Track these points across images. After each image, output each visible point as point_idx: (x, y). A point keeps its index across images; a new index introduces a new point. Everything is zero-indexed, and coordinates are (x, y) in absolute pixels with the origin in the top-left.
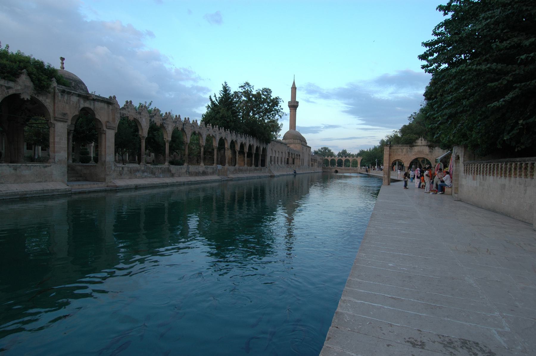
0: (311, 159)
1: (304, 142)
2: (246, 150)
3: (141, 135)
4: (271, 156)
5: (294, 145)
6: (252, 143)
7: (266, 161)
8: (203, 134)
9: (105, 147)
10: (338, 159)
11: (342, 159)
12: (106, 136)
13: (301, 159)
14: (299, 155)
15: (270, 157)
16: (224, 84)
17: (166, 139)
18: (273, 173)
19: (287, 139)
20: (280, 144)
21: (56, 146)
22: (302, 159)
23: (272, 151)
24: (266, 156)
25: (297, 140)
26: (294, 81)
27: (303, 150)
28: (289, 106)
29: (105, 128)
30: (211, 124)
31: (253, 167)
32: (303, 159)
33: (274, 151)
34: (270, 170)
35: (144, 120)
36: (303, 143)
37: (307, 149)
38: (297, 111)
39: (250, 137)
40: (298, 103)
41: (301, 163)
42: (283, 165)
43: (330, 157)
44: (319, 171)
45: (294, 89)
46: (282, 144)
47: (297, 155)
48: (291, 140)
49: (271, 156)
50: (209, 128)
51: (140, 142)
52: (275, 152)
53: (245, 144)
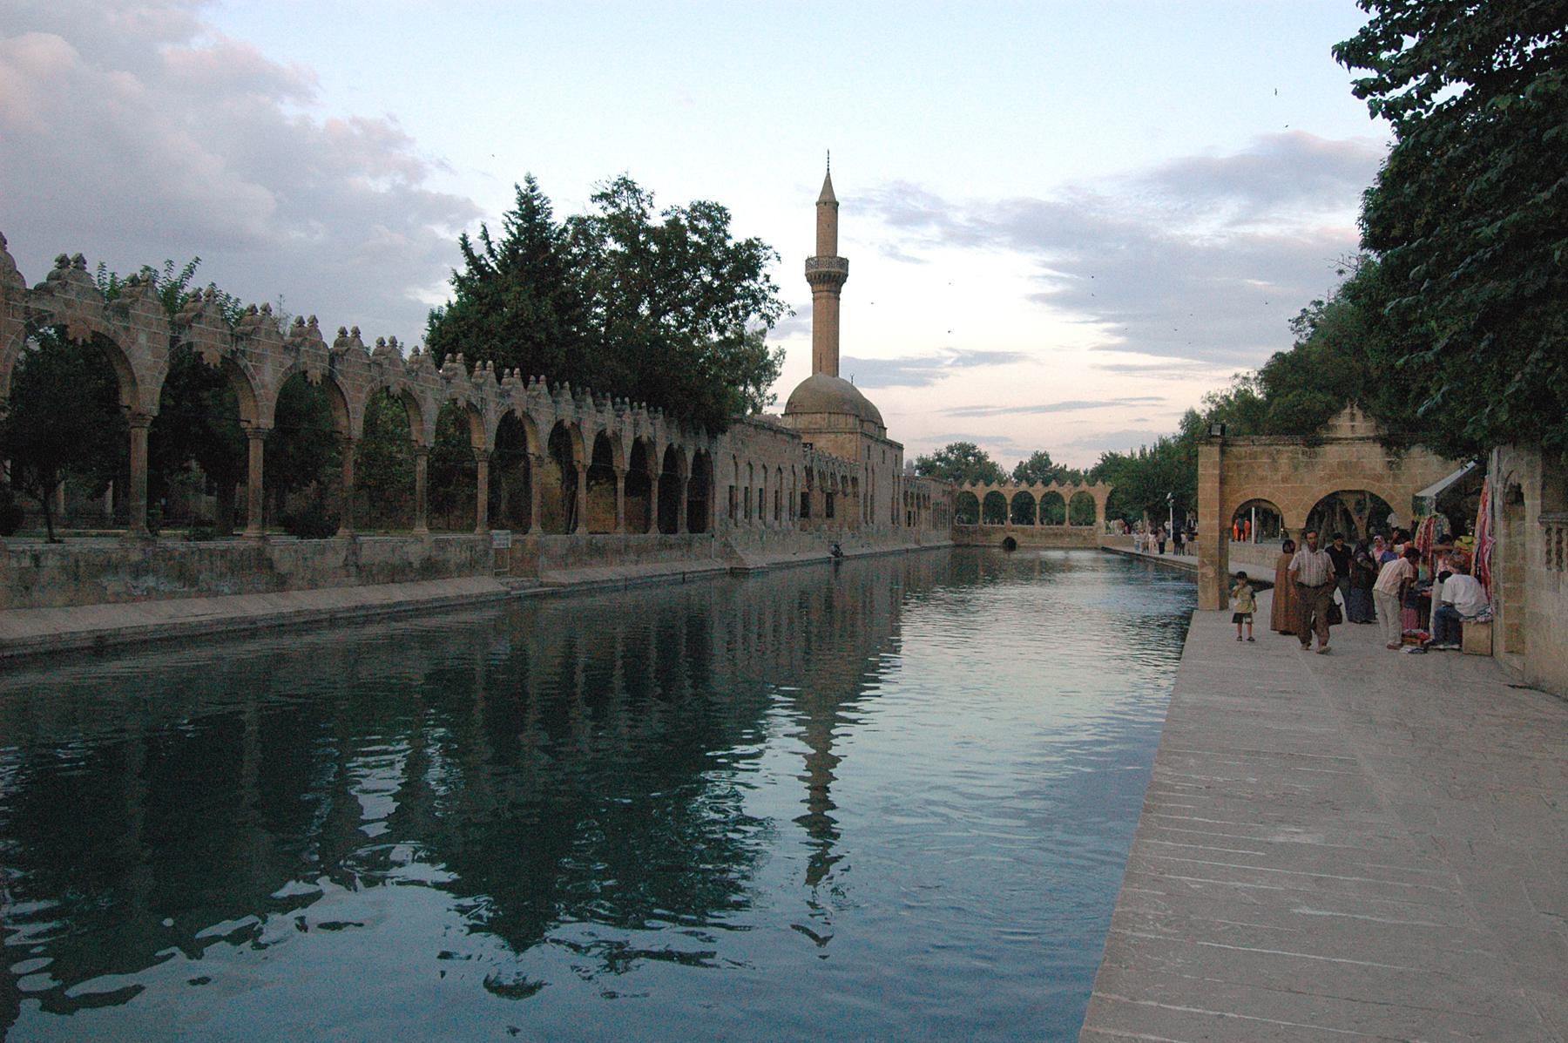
5: (833, 436)
6: (646, 432)
14: (855, 480)
16: (524, 186)
22: (866, 495)
25: (842, 419)
26: (828, 175)
33: (742, 466)
35: (142, 339)
37: (888, 455)
42: (784, 523)
43: (981, 484)
45: (828, 207)
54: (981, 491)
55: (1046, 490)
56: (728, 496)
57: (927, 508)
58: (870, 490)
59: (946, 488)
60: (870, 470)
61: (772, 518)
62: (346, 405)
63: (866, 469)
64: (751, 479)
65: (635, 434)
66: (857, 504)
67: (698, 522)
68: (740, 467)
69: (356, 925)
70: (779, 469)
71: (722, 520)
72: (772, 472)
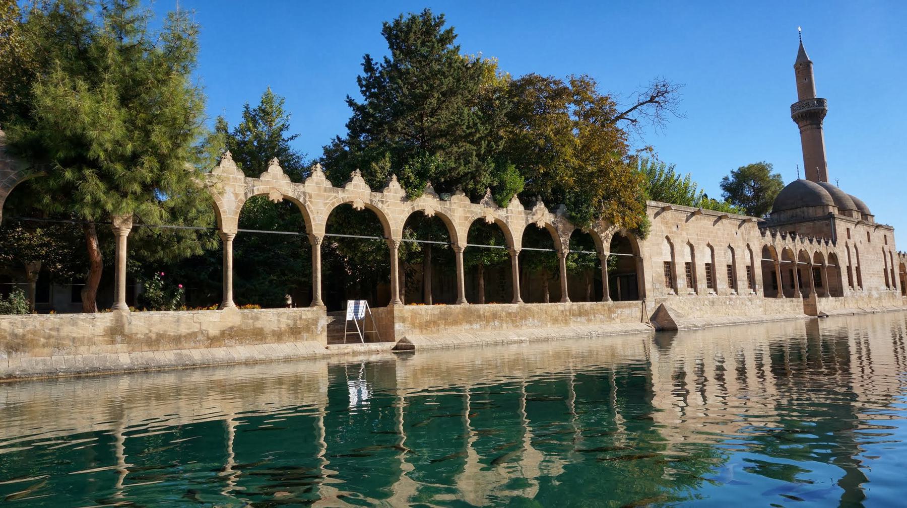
22: (849, 268)
26: (801, 45)
27: (849, 237)
28: (796, 118)
32: (858, 269)
40: (821, 101)
65: (527, 220)
68: (677, 248)
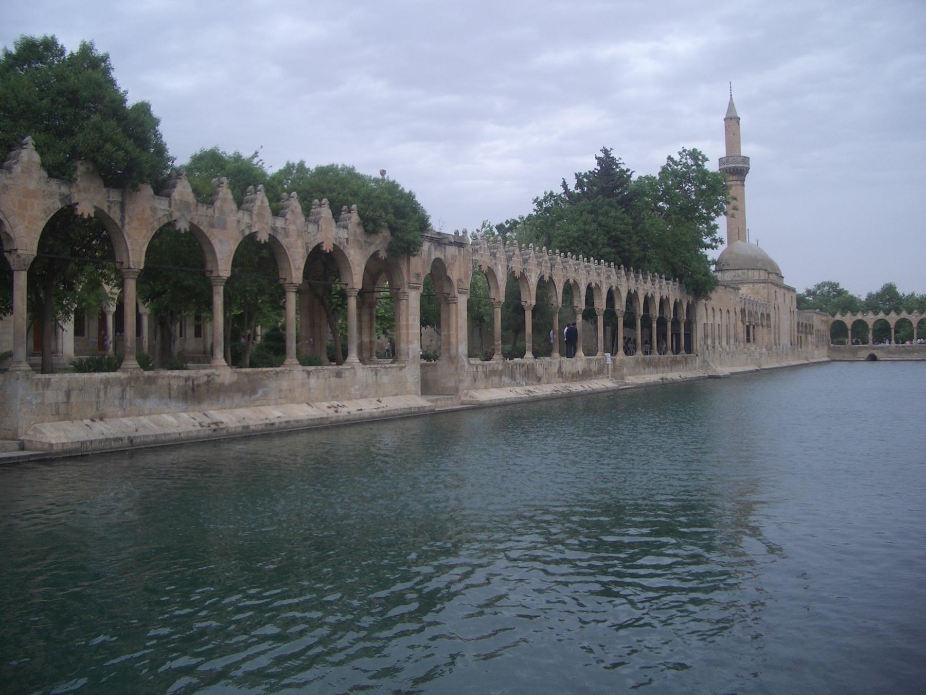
0: (798, 323)
1: (777, 274)
2: (601, 304)
3: (494, 299)
4: (704, 324)
5: (751, 285)
6: (665, 293)
7: (695, 339)
8: (581, 283)
9: (457, 328)
10: (873, 321)
11: (887, 318)
12: (457, 306)
13: (772, 326)
14: (768, 315)
15: (703, 326)
16: (602, 155)
17: (526, 302)
18: (715, 370)
19: (728, 270)
20: (723, 288)
21: (410, 331)
22: (775, 326)
23: (706, 309)
24: (694, 325)
25: (756, 273)
26: (731, 98)
27: (776, 300)
29: (457, 294)
30: (612, 263)
31: (670, 354)
32: (779, 327)
33: (710, 310)
34: (704, 361)
35: (500, 267)
36: (773, 277)
37: (787, 295)
38: (745, 183)
39: (554, 253)
41: (772, 336)
42: (732, 347)
43: (849, 314)
44: (820, 360)
45: (732, 121)
46: (728, 289)
47: (762, 315)
48: (740, 271)
49: (704, 324)
50: (589, 269)
51: (210, 289)
52: (712, 311)
53: (653, 297)
54: (849, 320)
55: (855, 319)
56: (703, 329)
57: (811, 334)
58: (777, 322)
59: (823, 319)
60: (776, 308)
61: (725, 343)
62: (529, 287)
63: (775, 308)
64: (714, 319)
66: (769, 333)
67: (689, 349)
69: (362, 670)
70: (728, 310)
71: (701, 345)
72: (724, 312)
